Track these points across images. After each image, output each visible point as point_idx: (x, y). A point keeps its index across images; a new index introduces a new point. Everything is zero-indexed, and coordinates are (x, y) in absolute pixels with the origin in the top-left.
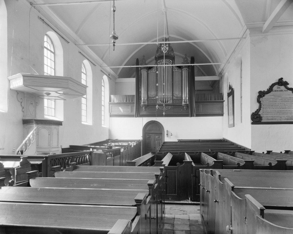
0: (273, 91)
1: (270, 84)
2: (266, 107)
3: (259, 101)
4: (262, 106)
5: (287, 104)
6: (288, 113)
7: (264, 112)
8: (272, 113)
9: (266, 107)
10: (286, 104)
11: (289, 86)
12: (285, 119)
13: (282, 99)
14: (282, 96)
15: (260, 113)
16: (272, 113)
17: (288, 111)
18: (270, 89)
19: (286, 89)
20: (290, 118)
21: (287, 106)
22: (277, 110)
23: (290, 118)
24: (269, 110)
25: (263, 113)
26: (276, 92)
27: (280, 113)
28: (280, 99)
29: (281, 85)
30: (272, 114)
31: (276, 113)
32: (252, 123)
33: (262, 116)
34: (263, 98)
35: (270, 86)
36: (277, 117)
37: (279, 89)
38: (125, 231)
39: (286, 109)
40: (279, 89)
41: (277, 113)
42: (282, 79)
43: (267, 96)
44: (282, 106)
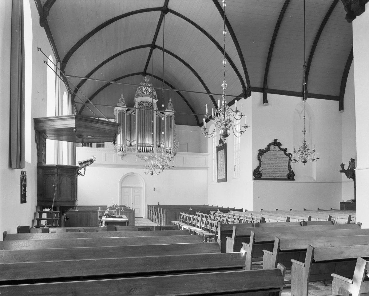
1: (268, 144)
3: (259, 159)
11: (282, 147)
14: (277, 155)
18: (268, 149)
19: (280, 150)
21: (280, 164)
39: (279, 168)
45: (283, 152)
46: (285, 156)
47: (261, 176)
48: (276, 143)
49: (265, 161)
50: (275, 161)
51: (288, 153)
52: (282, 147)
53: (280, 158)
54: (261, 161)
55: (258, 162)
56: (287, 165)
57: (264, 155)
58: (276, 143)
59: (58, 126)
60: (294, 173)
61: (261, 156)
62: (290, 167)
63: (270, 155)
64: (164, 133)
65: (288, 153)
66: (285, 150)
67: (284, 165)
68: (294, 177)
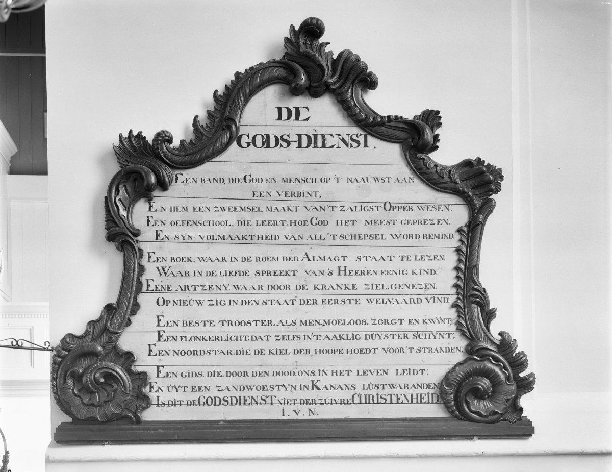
0: (245, 140)
1: (221, 80)
2: (185, 281)
3: (120, 235)
4: (151, 273)
5: (363, 265)
6: (369, 344)
7: (169, 331)
8: (234, 346)
9: (185, 281)
10: (352, 265)
11: (380, 102)
12: (347, 395)
13: (321, 216)
14: (321, 188)
15: (126, 342)
16: (234, 346)
17: (370, 328)
18: (219, 127)
19: (355, 131)
20: (388, 391)
21: (360, 281)
22: (277, 313)
23: (388, 391)
24: (217, 314)
25: (162, 346)
26: (274, 153)
27: (312, 345)
28: (302, 215)
29: (314, 91)
30: (239, 352)
31: (273, 344)
32: (63, 437)
33: (144, 363)
34: (160, 199)
35: (237, 75)
36: (281, 380)
37: (293, 129)
38: (6, 157)
39: (347, 312)
40: (293, 129)
41: (282, 345)
42: (312, 30)
43: (188, 188)
44: (320, 280)
45: (391, 152)
46: (421, 192)
47: (145, 401)
48: (309, 66)
49: (194, 251)
50: (300, 253)
51: (447, 155)
52: (380, 102)
53: (362, 216)
54: (146, 247)
55: (114, 259)
56: (445, 279)
57: (174, 189)
58: (309, 66)
59: (479, 234)
60: (518, 363)
61: (141, 207)
62: (471, 298)
63: (243, 190)
64: (161, 428)
65: (447, 155)
66: (415, 136)
67: (408, 279)
68: (525, 401)
